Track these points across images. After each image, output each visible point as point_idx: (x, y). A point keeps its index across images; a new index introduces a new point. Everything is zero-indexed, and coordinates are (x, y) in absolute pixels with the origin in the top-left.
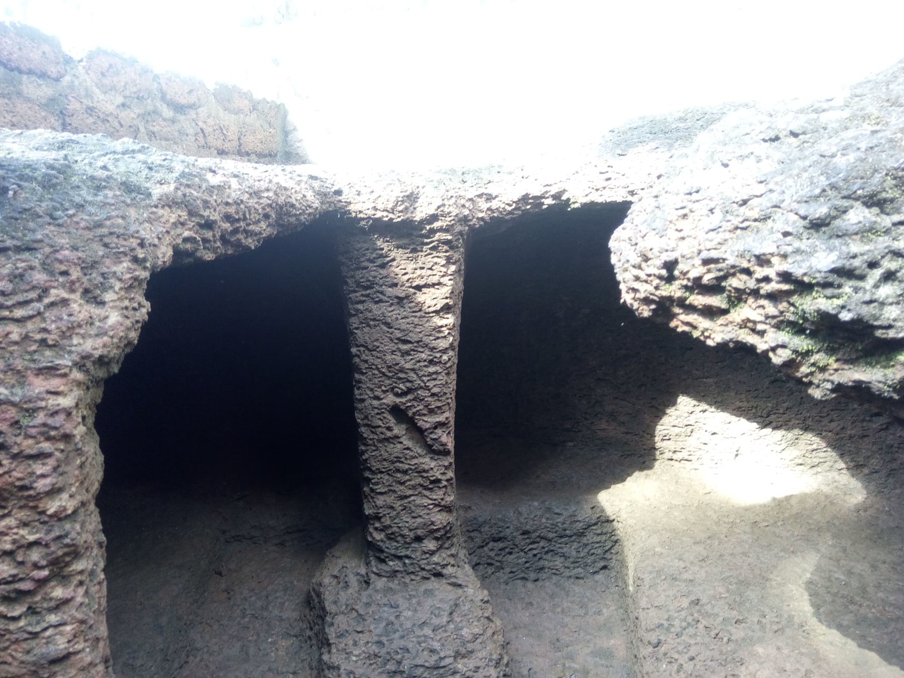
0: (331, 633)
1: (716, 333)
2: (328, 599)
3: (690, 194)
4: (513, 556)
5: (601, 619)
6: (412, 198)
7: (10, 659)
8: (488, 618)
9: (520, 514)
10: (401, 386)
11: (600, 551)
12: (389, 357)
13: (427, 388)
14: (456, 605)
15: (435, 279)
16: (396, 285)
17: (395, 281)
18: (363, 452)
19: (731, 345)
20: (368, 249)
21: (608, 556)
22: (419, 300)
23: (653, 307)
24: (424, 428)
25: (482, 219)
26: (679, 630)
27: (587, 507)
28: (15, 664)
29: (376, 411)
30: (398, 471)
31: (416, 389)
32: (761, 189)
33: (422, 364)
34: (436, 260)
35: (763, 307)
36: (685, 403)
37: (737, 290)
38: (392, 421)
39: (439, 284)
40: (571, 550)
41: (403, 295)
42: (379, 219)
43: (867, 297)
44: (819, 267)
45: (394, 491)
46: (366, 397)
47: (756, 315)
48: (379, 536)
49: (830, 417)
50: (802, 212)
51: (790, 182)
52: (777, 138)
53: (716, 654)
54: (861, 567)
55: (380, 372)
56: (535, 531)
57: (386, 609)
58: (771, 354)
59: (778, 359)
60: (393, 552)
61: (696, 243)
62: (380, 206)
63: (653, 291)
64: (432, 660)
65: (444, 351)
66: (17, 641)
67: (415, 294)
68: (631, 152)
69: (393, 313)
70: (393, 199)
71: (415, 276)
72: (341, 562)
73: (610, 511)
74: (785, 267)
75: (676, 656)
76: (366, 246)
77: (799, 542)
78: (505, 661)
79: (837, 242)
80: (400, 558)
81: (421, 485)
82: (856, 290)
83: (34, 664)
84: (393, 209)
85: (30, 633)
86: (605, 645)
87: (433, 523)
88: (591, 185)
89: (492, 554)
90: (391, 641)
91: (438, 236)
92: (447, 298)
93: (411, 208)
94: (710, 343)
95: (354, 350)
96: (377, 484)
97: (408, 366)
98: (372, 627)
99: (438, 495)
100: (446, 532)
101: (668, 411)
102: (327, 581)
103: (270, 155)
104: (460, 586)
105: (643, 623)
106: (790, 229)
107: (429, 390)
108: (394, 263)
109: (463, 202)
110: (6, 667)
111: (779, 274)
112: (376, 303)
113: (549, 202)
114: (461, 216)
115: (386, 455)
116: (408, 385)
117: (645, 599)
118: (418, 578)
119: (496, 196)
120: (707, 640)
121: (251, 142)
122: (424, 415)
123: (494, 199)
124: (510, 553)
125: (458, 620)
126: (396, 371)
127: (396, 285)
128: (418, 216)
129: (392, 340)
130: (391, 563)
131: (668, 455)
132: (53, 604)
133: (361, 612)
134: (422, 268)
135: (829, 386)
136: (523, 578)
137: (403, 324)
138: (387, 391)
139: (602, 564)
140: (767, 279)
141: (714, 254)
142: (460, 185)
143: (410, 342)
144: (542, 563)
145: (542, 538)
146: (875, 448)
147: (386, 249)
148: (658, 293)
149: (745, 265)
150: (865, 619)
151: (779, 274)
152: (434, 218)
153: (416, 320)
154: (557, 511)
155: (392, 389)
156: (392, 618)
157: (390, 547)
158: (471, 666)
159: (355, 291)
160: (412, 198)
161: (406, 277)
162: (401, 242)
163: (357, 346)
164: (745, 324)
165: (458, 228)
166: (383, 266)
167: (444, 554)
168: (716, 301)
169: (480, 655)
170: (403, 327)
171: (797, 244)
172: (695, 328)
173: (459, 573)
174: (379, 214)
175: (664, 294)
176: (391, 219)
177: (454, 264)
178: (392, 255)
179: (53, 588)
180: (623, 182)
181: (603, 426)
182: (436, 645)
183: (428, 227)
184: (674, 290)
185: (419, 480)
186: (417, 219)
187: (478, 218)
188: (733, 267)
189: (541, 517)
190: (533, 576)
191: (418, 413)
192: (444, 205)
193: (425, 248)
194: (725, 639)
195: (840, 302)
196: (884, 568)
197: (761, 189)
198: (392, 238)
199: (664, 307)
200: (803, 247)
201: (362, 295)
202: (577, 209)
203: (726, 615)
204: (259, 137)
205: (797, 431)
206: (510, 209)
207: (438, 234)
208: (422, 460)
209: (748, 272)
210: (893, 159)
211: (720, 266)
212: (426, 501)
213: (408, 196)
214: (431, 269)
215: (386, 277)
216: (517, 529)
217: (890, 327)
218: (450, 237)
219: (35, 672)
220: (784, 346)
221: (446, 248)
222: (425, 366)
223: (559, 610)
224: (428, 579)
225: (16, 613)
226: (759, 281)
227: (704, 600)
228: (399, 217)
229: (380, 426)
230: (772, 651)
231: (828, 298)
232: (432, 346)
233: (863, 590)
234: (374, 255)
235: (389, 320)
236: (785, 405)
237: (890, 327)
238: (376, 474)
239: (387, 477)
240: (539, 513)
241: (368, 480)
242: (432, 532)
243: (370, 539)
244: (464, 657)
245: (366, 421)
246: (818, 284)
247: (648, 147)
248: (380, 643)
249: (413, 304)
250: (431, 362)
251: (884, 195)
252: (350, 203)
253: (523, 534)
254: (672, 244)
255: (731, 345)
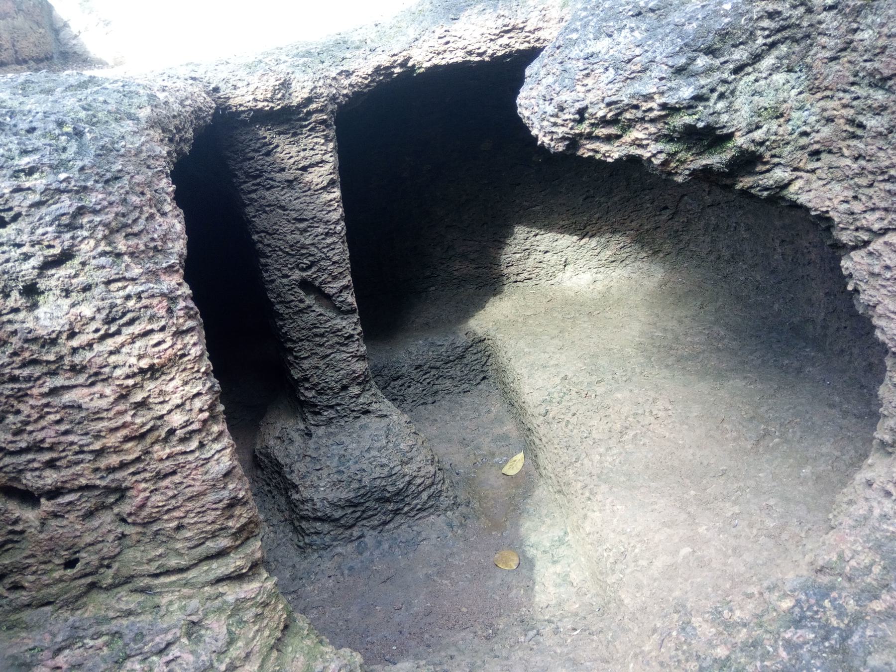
0: (295, 478)
1: (614, 152)
2: (279, 455)
3: (587, 58)
4: (412, 389)
5: (492, 416)
6: (285, 85)
7: (192, 483)
8: (415, 433)
9: (411, 353)
10: (305, 261)
11: (478, 366)
12: (289, 237)
13: (328, 258)
14: (388, 429)
15: (318, 158)
16: (283, 170)
17: (282, 166)
18: (282, 327)
19: (624, 158)
20: (251, 140)
21: (485, 368)
22: (307, 179)
23: (567, 143)
24: (331, 293)
25: (346, 95)
26: (559, 399)
27: (462, 334)
28: (198, 484)
29: (287, 288)
30: (316, 335)
31: (319, 261)
32: (638, 51)
33: (320, 237)
34: (315, 140)
35: (647, 129)
36: (521, 232)
37: (629, 120)
38: (302, 294)
39: (322, 162)
40: (456, 371)
41: (291, 178)
42: (261, 109)
43: (711, 111)
44: (685, 96)
45: (316, 354)
46: (275, 277)
47: (640, 135)
48: (310, 394)
49: (630, 219)
50: (670, 63)
51: (658, 44)
52: (640, 14)
53: (589, 406)
54: (671, 324)
55: (284, 252)
56: (425, 364)
57: (334, 447)
58: (653, 159)
59: (656, 162)
60: (325, 404)
61: (600, 92)
62: (260, 97)
63: (569, 131)
64: (386, 471)
65: (337, 223)
66: (196, 468)
67: (302, 175)
68: (463, 17)
69: (285, 197)
70: (271, 88)
71: (299, 158)
72: (279, 425)
73: (480, 333)
74: (663, 100)
75: (562, 417)
76: (249, 137)
77: (625, 319)
78: (436, 459)
79: (692, 80)
80: (332, 407)
81: (338, 343)
82: (705, 107)
83: (213, 479)
84: (271, 98)
85: (205, 459)
86: (501, 432)
87: (354, 372)
88: (431, 49)
89: (395, 391)
90: (349, 468)
91: (314, 117)
92: (331, 174)
93: (287, 95)
94: (610, 160)
95: (255, 237)
96: (300, 351)
97: (308, 242)
98: (328, 463)
99: (353, 348)
100: (366, 377)
101: (508, 241)
102: (272, 443)
103: (47, 59)
104: (385, 416)
105: (531, 404)
106: (664, 75)
107: (330, 259)
108: (279, 149)
109: (329, 81)
110: (191, 489)
111: (659, 105)
112: (268, 189)
113: (398, 70)
114: (331, 95)
115: (303, 325)
116: (311, 258)
117: (527, 387)
118: (351, 419)
119: (353, 72)
120: (580, 400)
121: (26, 48)
122: (329, 282)
123: (352, 74)
124: (409, 387)
125: (394, 440)
126: (298, 249)
127: (283, 170)
128: (295, 101)
129: (289, 221)
130: (325, 413)
131: (513, 278)
132: (214, 436)
133: (314, 455)
134: (304, 150)
135: (687, 172)
136: (423, 404)
137: (297, 204)
138: (293, 268)
139: (482, 376)
140: (651, 110)
141: (614, 98)
142: (321, 66)
143: (306, 220)
144: (435, 388)
145: (432, 368)
146: (666, 235)
147: (269, 137)
148: (572, 132)
149: (635, 102)
150: (682, 357)
151: (659, 105)
152: (309, 101)
153: (308, 199)
154: (439, 343)
155: (297, 266)
156: (342, 452)
157: (322, 400)
158: (415, 468)
159: (245, 182)
160: (285, 85)
161: (292, 161)
162: (281, 129)
163: (258, 233)
164: (633, 143)
165: (330, 107)
166: (268, 154)
167: (367, 395)
168: (613, 130)
169: (418, 459)
170: (298, 207)
171: (669, 84)
172: (597, 152)
173: (382, 407)
174: (260, 105)
175: (577, 132)
176: (272, 108)
177: (331, 141)
178: (275, 141)
179: (210, 425)
180: (461, 44)
181: (457, 267)
182: (384, 461)
183: (305, 111)
184: (585, 128)
185: (336, 339)
186: (295, 104)
187: (343, 95)
188: (628, 105)
189: (428, 351)
190: (430, 399)
191: (324, 282)
192: (315, 87)
193: (304, 130)
194: (593, 396)
195: (696, 117)
196: (687, 321)
197: (638, 51)
198: (273, 125)
199: (574, 142)
200: (673, 86)
201: (254, 185)
202: (423, 73)
203: (589, 380)
204: (31, 40)
205: (607, 236)
206: (366, 82)
207: (314, 115)
208: (334, 322)
209: (636, 107)
210: (717, 24)
211: (618, 106)
212: (344, 356)
213: (282, 84)
214: (312, 149)
215: (273, 164)
216: (411, 366)
217: (724, 127)
218: (325, 117)
219: (214, 485)
220: (661, 152)
221: (323, 127)
222: (323, 239)
223: (458, 418)
224: (359, 417)
225: (192, 448)
226: (644, 111)
227: (570, 375)
228: (279, 105)
229: (293, 301)
230: (627, 394)
231: (689, 115)
232: (325, 219)
233: (677, 338)
234: (258, 145)
235: (283, 203)
236: (596, 216)
237: (724, 127)
238: (297, 343)
239: (307, 343)
240: (425, 349)
241: (291, 350)
242: (354, 379)
243: (302, 399)
244: (407, 464)
245: (279, 299)
246: (684, 108)
247: (476, 11)
248: (340, 472)
249: (302, 185)
250: (327, 234)
251: (715, 46)
252: (229, 98)
253: (416, 369)
254: (582, 95)
255: (624, 158)
